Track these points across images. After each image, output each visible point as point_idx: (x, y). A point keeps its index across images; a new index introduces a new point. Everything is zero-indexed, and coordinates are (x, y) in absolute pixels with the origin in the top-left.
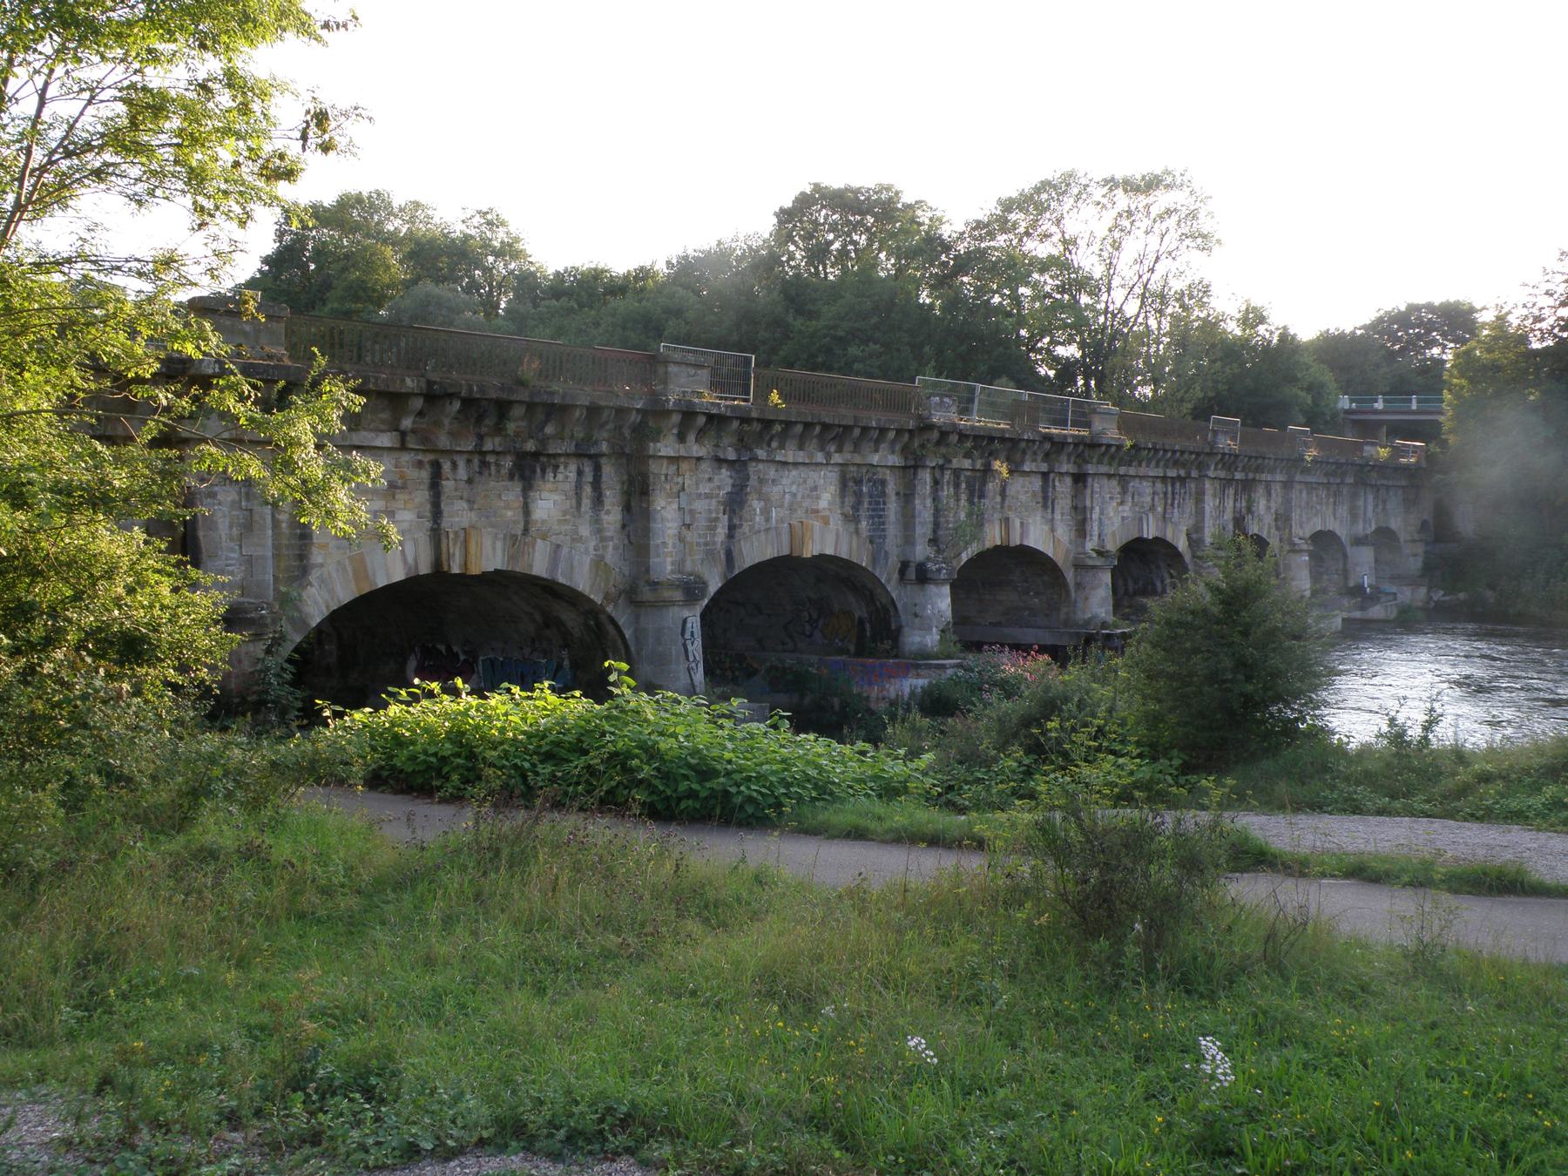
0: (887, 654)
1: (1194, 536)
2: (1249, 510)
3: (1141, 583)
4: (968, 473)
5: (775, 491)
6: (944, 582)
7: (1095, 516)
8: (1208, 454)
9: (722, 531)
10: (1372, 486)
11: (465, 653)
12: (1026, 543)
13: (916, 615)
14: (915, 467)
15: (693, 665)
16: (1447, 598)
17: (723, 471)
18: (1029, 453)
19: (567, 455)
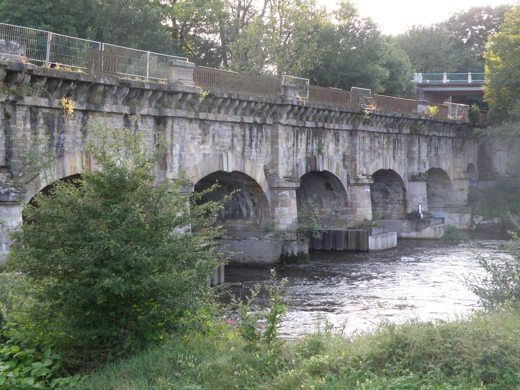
1: (271, 171)
2: (319, 151)
3: (231, 209)
4: (47, 111)
7: (176, 151)
8: (280, 106)
10: (426, 136)
16: (485, 222)
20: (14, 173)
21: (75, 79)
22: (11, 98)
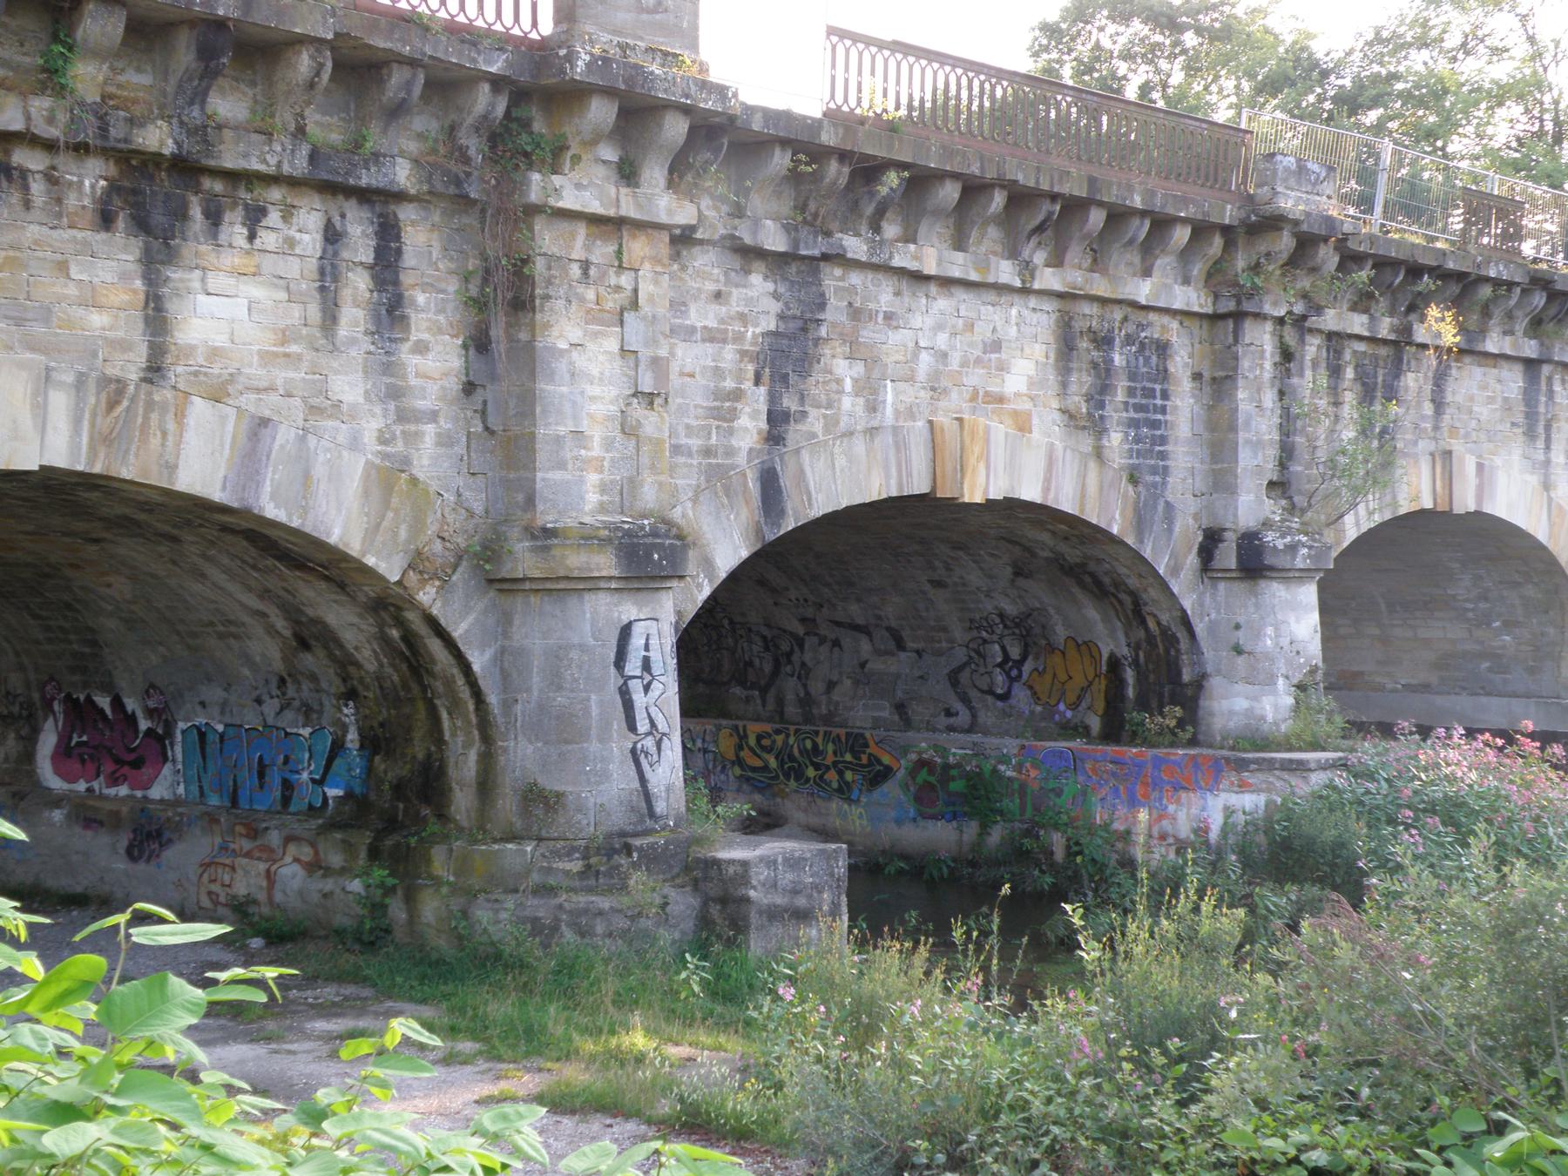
0: (1171, 737)
4: (1361, 347)
5: (894, 343)
6: (1303, 575)
9: (750, 425)
11: (151, 713)
12: (1488, 509)
13: (1238, 650)
14: (1238, 316)
15: (649, 743)
17: (756, 279)
18: (1498, 313)
19: (293, 182)
20: (1296, 499)
21: (1435, 264)
22: (1299, 308)
